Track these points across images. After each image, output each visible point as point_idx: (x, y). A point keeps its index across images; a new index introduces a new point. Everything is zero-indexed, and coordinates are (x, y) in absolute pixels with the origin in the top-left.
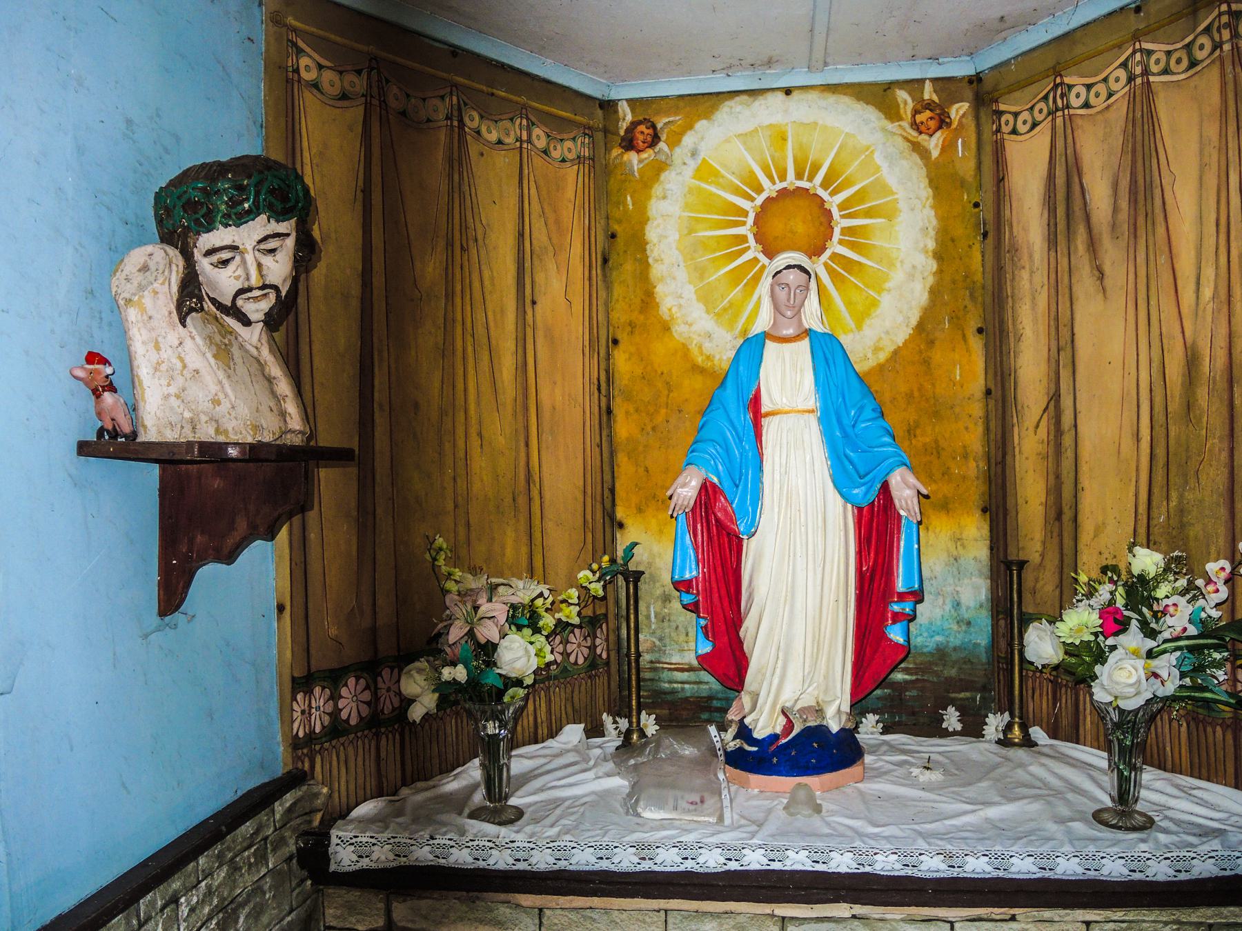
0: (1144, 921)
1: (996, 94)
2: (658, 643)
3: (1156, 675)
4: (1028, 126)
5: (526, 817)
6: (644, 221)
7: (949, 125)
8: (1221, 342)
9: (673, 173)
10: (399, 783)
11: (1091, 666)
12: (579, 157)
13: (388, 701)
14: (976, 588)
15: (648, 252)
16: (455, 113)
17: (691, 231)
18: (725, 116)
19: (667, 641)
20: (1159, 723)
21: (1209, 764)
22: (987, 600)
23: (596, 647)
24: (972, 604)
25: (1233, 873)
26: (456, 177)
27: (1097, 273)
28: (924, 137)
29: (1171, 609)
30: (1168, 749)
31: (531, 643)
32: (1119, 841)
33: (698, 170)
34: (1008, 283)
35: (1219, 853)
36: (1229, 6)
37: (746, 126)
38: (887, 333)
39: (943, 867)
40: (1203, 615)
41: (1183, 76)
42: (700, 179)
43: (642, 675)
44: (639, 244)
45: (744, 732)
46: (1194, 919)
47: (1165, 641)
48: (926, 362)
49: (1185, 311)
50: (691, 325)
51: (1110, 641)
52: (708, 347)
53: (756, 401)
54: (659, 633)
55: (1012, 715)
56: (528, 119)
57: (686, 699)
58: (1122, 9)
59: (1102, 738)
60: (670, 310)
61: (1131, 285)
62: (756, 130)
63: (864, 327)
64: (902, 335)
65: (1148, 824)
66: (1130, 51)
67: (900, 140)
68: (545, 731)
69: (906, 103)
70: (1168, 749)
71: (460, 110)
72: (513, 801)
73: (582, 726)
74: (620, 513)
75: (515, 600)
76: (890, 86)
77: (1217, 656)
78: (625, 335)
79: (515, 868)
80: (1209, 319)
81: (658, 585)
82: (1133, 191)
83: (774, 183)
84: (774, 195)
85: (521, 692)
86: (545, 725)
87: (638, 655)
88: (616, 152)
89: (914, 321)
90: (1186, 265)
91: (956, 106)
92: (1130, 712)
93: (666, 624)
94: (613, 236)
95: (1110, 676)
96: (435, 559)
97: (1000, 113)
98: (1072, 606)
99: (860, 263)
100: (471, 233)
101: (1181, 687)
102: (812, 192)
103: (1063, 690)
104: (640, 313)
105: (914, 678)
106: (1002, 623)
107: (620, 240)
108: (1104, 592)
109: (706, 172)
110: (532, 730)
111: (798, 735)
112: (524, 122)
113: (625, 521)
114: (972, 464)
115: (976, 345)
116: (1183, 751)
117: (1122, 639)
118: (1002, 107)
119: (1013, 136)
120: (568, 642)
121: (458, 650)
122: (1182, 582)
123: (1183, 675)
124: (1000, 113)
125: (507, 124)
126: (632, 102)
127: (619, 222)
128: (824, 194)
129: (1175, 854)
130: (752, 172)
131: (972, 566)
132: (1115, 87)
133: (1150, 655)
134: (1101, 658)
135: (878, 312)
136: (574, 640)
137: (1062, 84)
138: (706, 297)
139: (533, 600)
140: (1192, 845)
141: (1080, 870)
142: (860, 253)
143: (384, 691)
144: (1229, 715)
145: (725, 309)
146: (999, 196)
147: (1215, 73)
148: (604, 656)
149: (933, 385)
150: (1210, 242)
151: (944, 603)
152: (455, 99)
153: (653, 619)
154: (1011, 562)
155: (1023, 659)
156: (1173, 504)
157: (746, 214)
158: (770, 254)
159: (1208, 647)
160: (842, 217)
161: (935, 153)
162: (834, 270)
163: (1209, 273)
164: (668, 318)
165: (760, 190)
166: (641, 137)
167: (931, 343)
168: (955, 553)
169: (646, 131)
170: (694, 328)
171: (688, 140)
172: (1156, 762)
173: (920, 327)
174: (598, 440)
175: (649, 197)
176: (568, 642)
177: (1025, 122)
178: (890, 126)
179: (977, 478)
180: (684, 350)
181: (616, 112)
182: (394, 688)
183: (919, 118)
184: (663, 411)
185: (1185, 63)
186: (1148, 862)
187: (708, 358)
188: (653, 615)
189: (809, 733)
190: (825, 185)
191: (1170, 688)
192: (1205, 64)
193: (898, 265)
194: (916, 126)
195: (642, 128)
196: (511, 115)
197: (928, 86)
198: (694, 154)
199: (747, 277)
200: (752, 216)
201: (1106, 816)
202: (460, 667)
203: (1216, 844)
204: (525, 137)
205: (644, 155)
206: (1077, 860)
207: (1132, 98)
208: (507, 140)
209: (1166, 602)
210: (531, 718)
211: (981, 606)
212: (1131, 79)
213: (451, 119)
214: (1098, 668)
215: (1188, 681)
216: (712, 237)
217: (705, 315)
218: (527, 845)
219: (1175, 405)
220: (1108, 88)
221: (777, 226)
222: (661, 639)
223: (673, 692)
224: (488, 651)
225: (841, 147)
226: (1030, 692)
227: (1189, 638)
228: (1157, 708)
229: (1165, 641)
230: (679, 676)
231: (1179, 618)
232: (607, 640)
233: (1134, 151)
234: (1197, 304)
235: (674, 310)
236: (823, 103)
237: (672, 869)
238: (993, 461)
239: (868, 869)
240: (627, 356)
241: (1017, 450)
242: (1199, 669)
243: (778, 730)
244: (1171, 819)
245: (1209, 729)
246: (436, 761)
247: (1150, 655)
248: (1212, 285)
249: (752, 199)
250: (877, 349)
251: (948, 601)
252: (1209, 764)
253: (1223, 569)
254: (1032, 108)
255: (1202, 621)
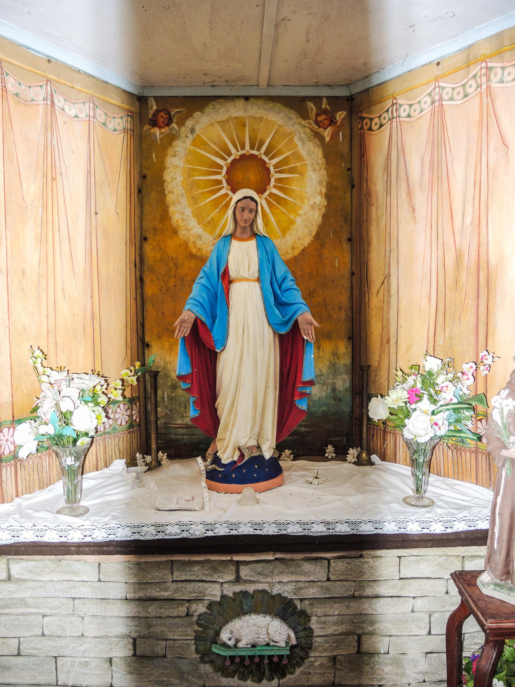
0: (429, 555)
1: (361, 108)
2: (169, 413)
3: (436, 424)
4: (378, 126)
5: (90, 512)
6: (162, 168)
7: (335, 123)
8: (474, 247)
9: (180, 142)
10: (14, 495)
11: (402, 420)
12: (124, 129)
13: (7, 447)
14: (344, 380)
15: (165, 187)
16: (49, 97)
17: (190, 176)
18: (210, 110)
19: (174, 411)
20: (437, 451)
21: (463, 472)
22: (349, 387)
23: (132, 415)
24: (342, 389)
25: (475, 528)
26: (49, 135)
27: (411, 209)
28: (321, 129)
29: (445, 389)
30: (442, 465)
31: (94, 411)
32: (416, 513)
33: (194, 141)
34: (365, 214)
35: (468, 518)
36: (487, 64)
37: (222, 117)
38: (299, 239)
39: (324, 529)
40: (461, 393)
41: (460, 102)
42: (195, 146)
43: (159, 431)
44: (160, 182)
45: (216, 460)
46: (455, 553)
47: (441, 406)
48: (320, 256)
49: (456, 230)
50: (189, 231)
51: (413, 406)
52: (199, 243)
53: (226, 272)
54: (169, 407)
55: (362, 449)
56: (94, 103)
57: (185, 444)
58: (430, 63)
59: (408, 460)
60: (177, 221)
61: (429, 217)
62: (228, 119)
63: (287, 235)
64: (307, 241)
65: (431, 504)
66: (433, 87)
67: (308, 130)
68: (103, 464)
69: (312, 109)
70: (442, 465)
71: (52, 95)
72: (83, 503)
73: (125, 460)
74: (147, 339)
75: (84, 386)
76: (305, 99)
77: (467, 414)
78: (151, 235)
79: (84, 541)
80: (468, 235)
81: (169, 379)
82: (431, 166)
83: (238, 151)
84: (238, 157)
85: (87, 440)
86: (102, 460)
87: (157, 419)
88: (146, 127)
89: (314, 233)
90: (457, 206)
91: (340, 113)
92: (423, 444)
93: (174, 402)
94: (144, 177)
95: (413, 424)
96: (35, 363)
97: (363, 118)
98: (394, 388)
99: (285, 199)
100: (58, 169)
101: (449, 430)
102: (259, 157)
103: (389, 434)
104: (160, 222)
105: (311, 430)
106: (357, 399)
107: (149, 179)
108: (411, 380)
109: (199, 142)
110: (95, 463)
111: (247, 461)
112: (92, 105)
113: (150, 343)
114: (343, 313)
115: (346, 246)
116: (450, 465)
117: (419, 405)
118: (364, 115)
119: (370, 132)
120: (116, 412)
121: (49, 416)
122: (450, 376)
123: (450, 424)
124: (363, 118)
125: (81, 105)
126: (157, 99)
127: (148, 168)
128: (266, 159)
129: (445, 519)
130: (225, 144)
131: (342, 369)
132: (424, 106)
133: (433, 413)
134: (408, 416)
135: (294, 227)
136: (120, 411)
137: (396, 103)
138: (198, 215)
139: (94, 387)
140: (453, 514)
141: (396, 529)
142: (285, 194)
143: (4, 442)
144: (474, 446)
145: (209, 222)
146: (361, 165)
147: (477, 100)
148: (138, 420)
149: (324, 269)
150: (470, 193)
151: (327, 389)
152: (49, 88)
153: (166, 399)
154: (363, 366)
155: (369, 419)
156: (447, 334)
157: (221, 168)
158: (234, 191)
159: (463, 409)
160: (276, 172)
161: (327, 139)
162: (271, 202)
163: (469, 210)
164: (176, 226)
165: (229, 154)
166: (161, 120)
167: (323, 245)
168: (333, 362)
169: (165, 116)
170: (192, 232)
171: (189, 123)
172: (436, 472)
173: (317, 236)
174: (134, 296)
175: (166, 155)
176: (116, 412)
177: (376, 124)
178: (303, 122)
179: (346, 320)
180: (185, 245)
181: (147, 104)
182: (11, 439)
183: (320, 118)
184: (173, 280)
185: (462, 95)
186: (431, 524)
187: (199, 250)
188: (166, 396)
189: (253, 460)
190: (266, 153)
191: (443, 431)
192: (472, 95)
193: (306, 201)
194: (317, 123)
195: (162, 114)
196: (83, 101)
197: (324, 101)
198: (192, 131)
199: (222, 204)
200: (225, 169)
201: (409, 500)
202: (50, 426)
203: (466, 513)
204: (92, 114)
205: (163, 130)
206: (395, 523)
207: (433, 114)
208: (80, 116)
209: (442, 385)
210: (94, 457)
211: (347, 390)
212: (433, 103)
213: (46, 100)
214: (406, 421)
215: (452, 428)
216: (202, 180)
217: (197, 225)
218: (91, 527)
219: (450, 281)
220: (421, 107)
221: (239, 176)
222: (170, 411)
223: (177, 440)
224: (65, 418)
225: (275, 133)
226: (371, 437)
227: (453, 404)
228: (435, 443)
229: (441, 406)
230: (181, 431)
231: (449, 395)
232: (139, 411)
233: (433, 143)
234: (463, 227)
235: (180, 221)
236: (266, 107)
237: (175, 537)
238: (354, 311)
239: (284, 532)
240: (151, 247)
241: (367, 305)
242: (458, 421)
243: (236, 458)
244: (443, 501)
245: (463, 453)
246: (37, 482)
247: (433, 413)
248: (470, 217)
249: (226, 160)
250: (293, 248)
251: (329, 387)
252: (463, 472)
253: (471, 367)
254: (380, 116)
255: (460, 396)
